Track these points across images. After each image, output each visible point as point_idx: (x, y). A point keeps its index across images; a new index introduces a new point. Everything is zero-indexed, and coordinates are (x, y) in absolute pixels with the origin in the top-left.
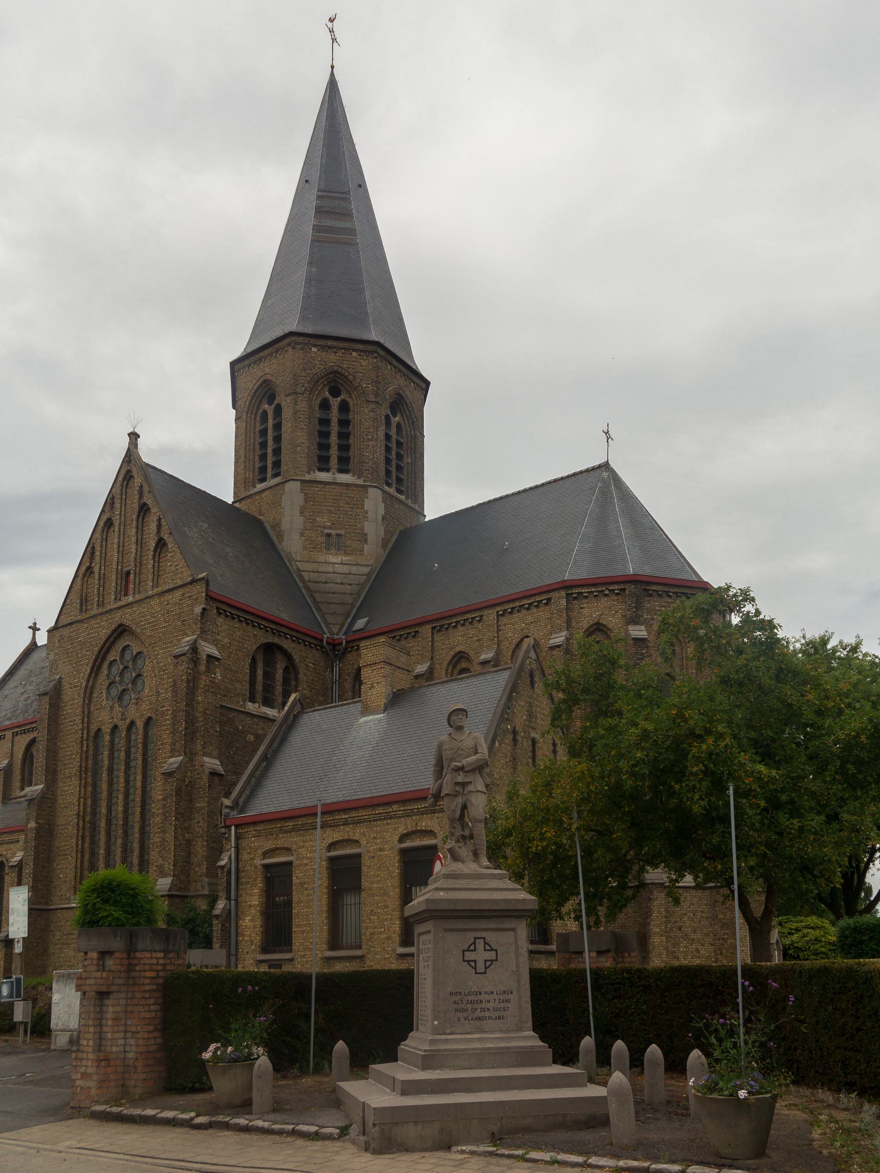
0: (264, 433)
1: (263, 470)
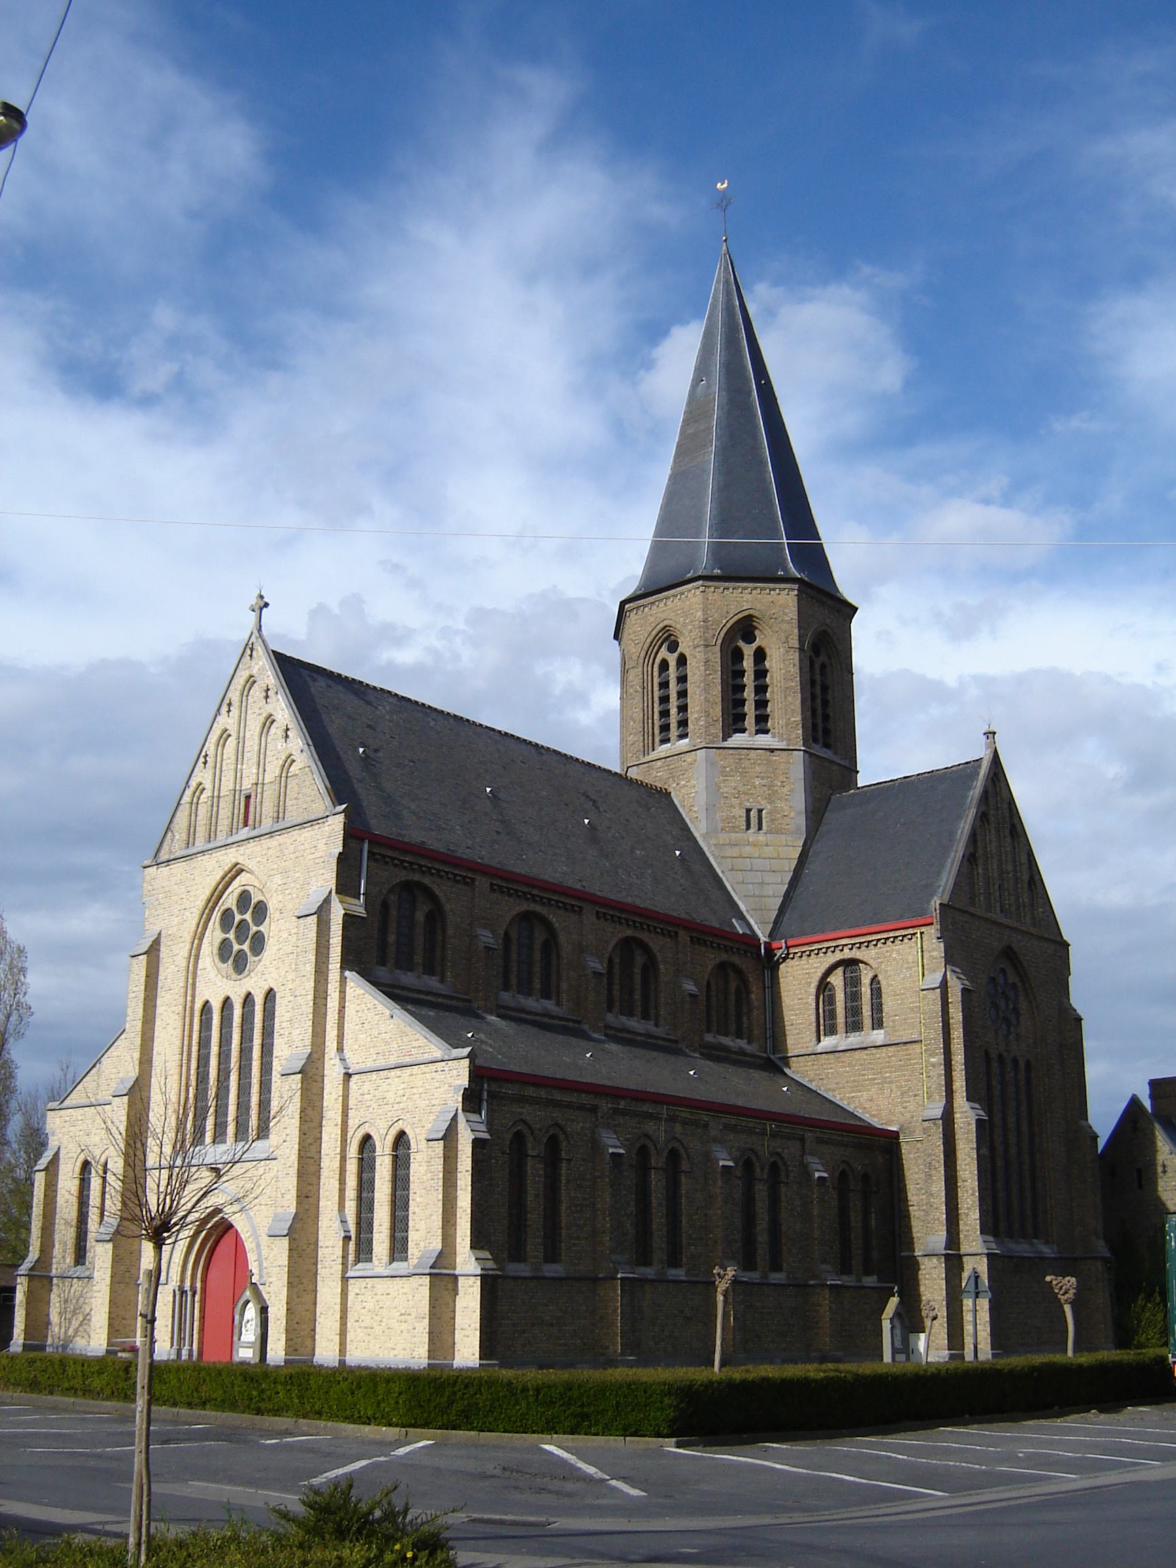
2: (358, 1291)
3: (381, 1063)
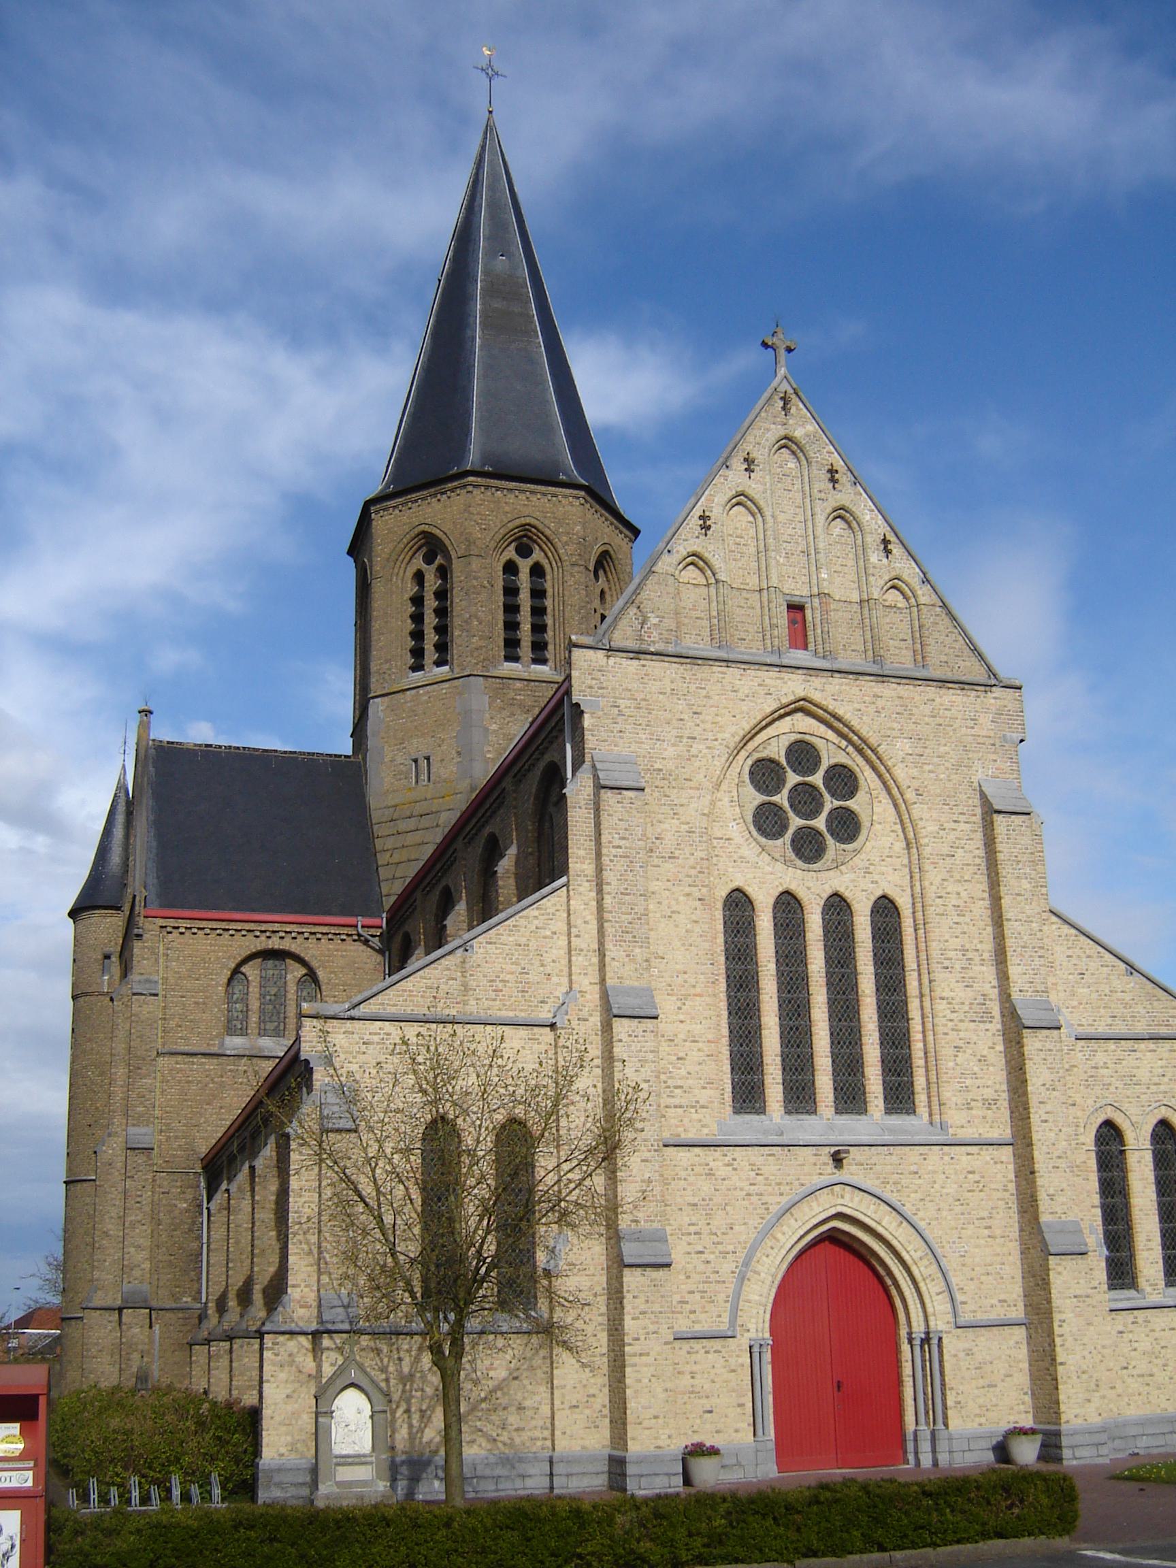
0: (418, 601)
1: (418, 653)
2: (1121, 1328)
3: (1120, 1029)
